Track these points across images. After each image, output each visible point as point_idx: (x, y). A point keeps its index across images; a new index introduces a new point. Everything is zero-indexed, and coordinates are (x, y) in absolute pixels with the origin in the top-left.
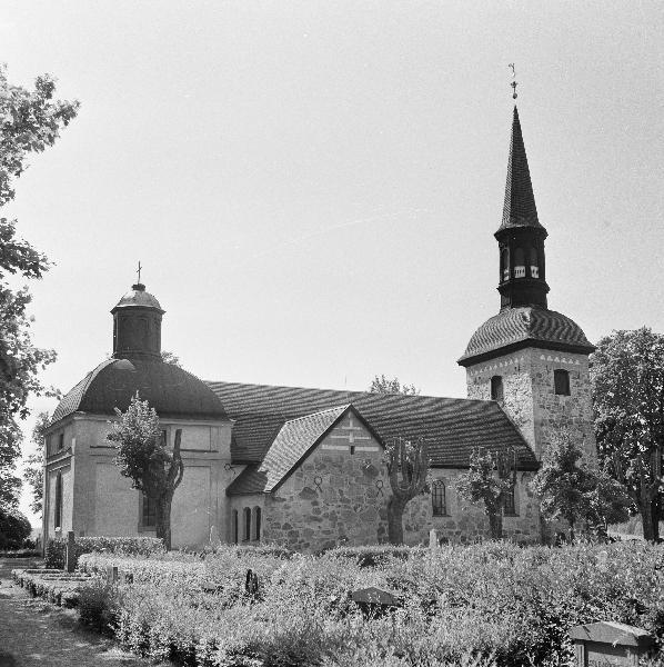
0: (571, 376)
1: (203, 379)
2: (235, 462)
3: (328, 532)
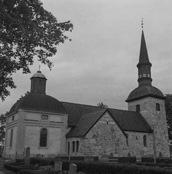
1: (60, 100)
2: (69, 126)
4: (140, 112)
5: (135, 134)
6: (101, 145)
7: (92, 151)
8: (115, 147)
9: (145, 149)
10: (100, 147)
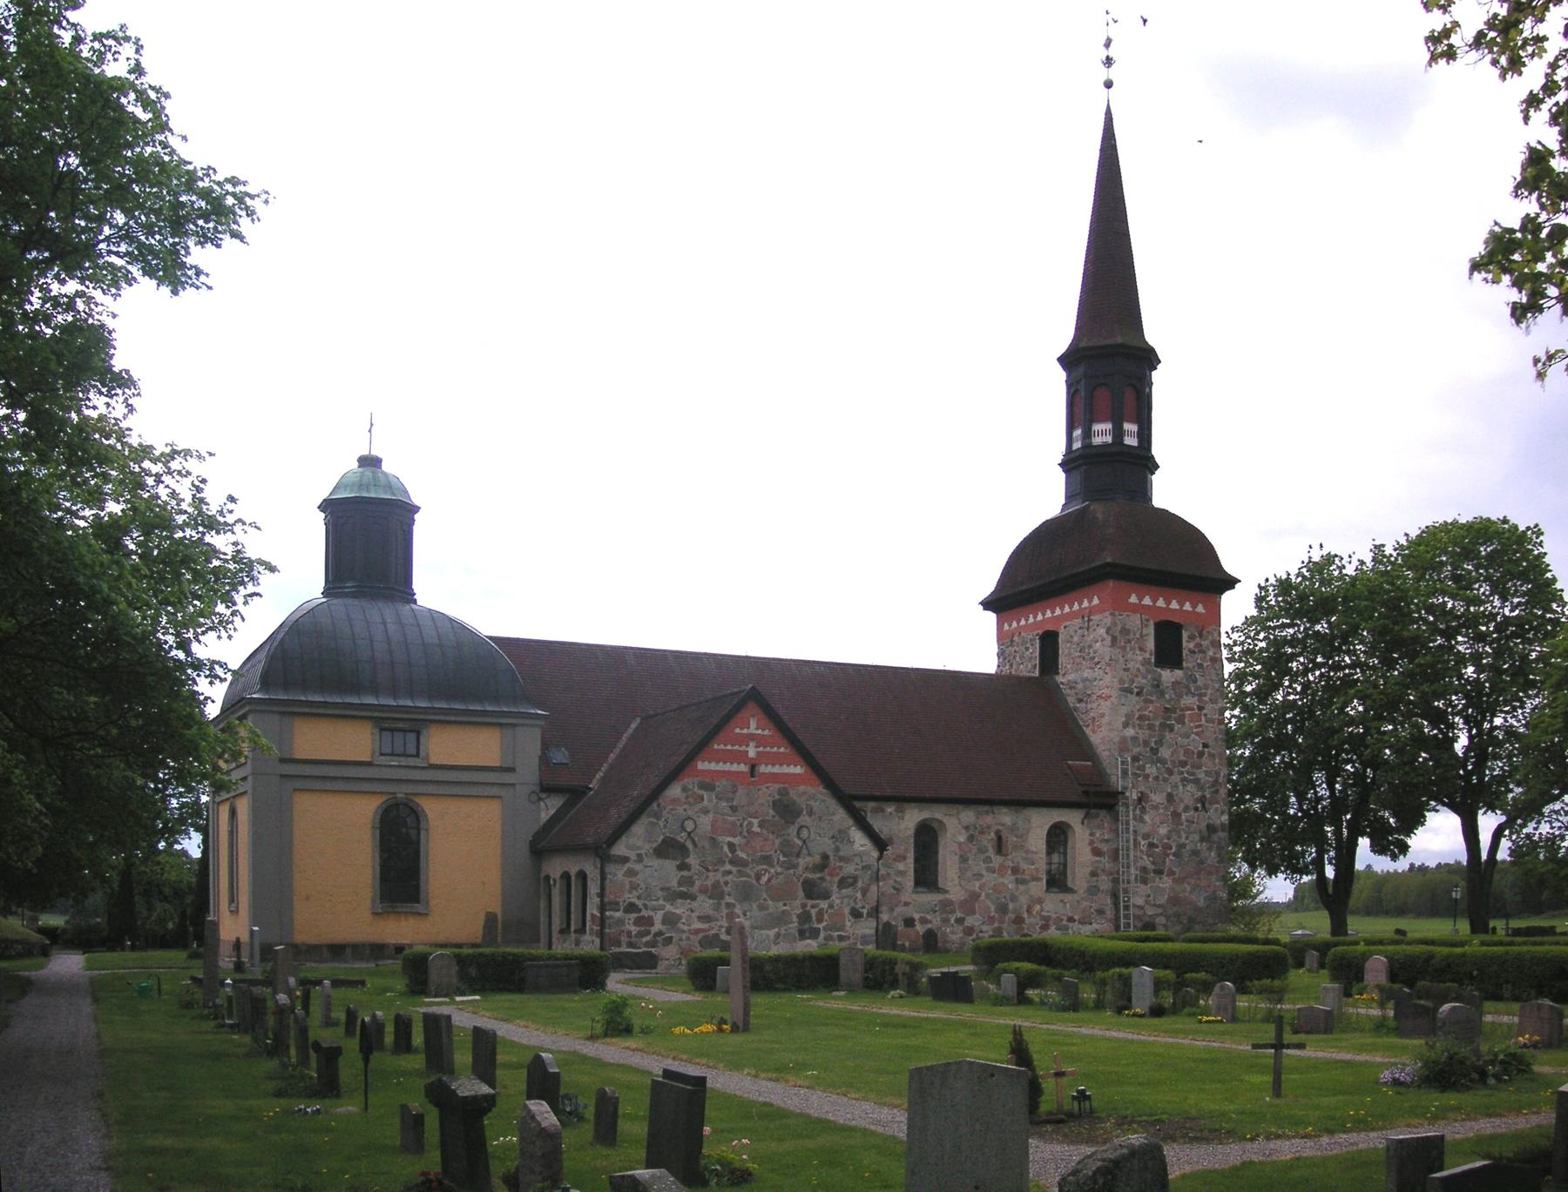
0: (1185, 635)
3: (705, 918)
4: (1059, 679)
5: (989, 819)
6: (716, 893)
7: (654, 929)
8: (798, 902)
9: (1054, 904)
10: (705, 904)
